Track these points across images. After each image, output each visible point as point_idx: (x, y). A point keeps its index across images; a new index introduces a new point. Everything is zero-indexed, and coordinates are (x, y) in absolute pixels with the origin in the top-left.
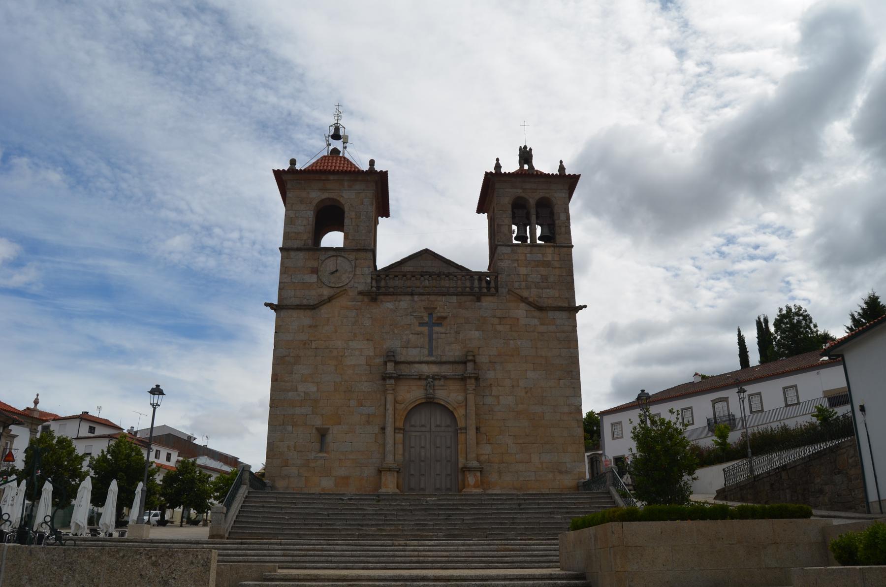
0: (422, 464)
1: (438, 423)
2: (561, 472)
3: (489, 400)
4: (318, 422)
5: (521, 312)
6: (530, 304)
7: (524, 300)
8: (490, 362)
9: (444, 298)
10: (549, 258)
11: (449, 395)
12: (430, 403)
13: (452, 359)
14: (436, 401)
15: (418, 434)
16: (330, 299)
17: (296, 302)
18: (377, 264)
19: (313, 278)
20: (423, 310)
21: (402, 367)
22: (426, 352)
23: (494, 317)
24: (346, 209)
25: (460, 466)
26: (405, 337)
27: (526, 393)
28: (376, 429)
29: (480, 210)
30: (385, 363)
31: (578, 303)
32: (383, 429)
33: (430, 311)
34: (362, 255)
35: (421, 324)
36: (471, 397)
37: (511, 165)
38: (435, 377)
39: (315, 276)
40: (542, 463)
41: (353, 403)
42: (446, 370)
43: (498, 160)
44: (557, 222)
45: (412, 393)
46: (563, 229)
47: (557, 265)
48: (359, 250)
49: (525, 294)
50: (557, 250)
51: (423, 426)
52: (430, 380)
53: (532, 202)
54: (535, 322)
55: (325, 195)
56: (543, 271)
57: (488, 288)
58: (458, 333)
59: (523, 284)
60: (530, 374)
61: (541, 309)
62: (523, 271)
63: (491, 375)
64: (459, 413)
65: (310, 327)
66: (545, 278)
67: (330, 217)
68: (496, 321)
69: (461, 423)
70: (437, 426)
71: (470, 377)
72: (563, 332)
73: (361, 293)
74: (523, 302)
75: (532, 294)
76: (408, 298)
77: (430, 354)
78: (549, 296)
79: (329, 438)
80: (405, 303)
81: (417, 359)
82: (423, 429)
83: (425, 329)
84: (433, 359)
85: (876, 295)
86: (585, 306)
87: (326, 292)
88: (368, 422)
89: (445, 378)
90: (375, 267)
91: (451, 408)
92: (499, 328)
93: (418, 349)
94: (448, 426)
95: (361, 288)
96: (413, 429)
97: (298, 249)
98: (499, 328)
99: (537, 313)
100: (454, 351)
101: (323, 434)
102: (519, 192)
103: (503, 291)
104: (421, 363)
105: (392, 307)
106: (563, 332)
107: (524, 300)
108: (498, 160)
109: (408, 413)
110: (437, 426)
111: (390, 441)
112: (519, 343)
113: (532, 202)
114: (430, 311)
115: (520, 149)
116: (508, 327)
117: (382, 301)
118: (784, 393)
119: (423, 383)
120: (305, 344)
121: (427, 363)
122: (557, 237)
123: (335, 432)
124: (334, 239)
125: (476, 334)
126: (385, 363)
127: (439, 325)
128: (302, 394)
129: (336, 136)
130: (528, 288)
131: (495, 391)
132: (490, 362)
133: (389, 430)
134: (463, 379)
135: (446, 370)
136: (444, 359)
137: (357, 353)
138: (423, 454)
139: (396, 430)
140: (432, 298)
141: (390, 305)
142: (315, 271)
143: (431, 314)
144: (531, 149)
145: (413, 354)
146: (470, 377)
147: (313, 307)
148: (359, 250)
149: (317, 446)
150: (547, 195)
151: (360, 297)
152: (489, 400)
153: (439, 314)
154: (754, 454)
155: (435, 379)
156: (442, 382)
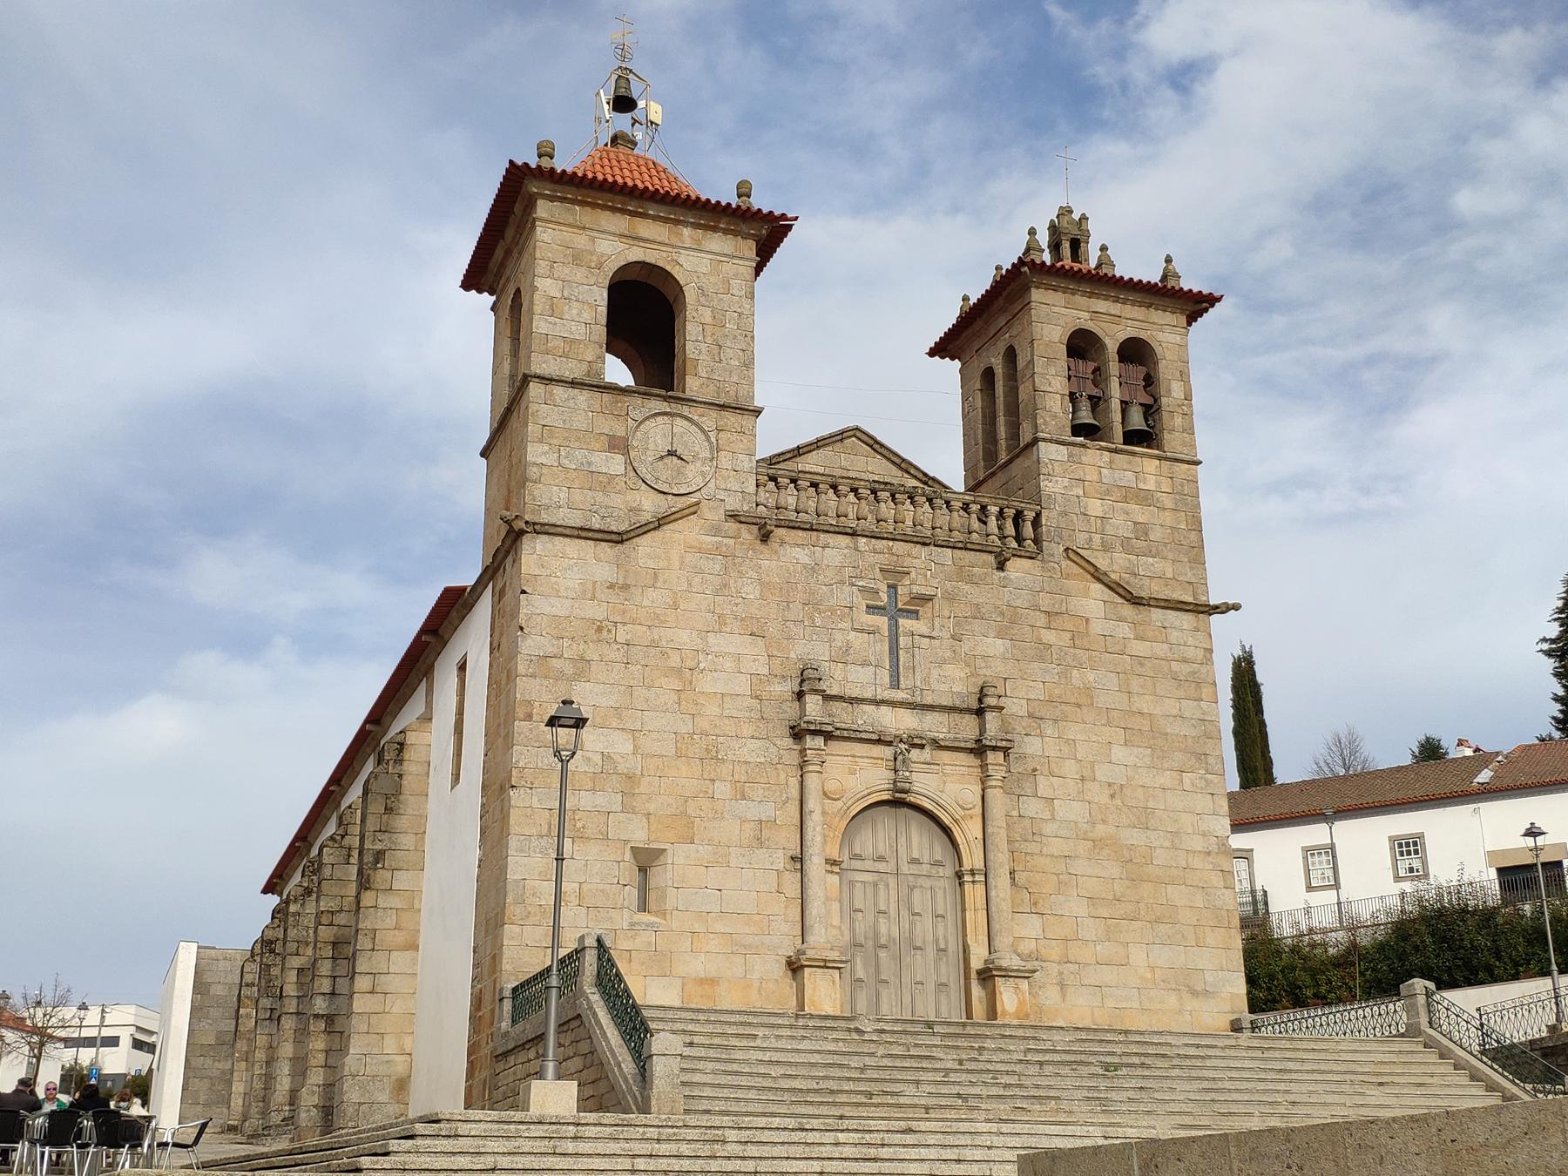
0: (883, 954)
1: (915, 855)
2: (1194, 993)
3: (1031, 807)
4: (639, 834)
5: (1093, 601)
6: (1113, 587)
7: (1098, 576)
8: (1031, 716)
9: (924, 551)
10: (1150, 485)
11: (946, 784)
12: (899, 801)
13: (946, 701)
14: (911, 798)
15: (868, 877)
16: (660, 522)
17: (575, 519)
19: (616, 464)
20: (878, 575)
21: (837, 707)
22: (886, 678)
23: (1036, 608)
24: (690, 295)
25: (976, 964)
26: (838, 636)
27: (1112, 796)
28: (780, 860)
29: (472, 281)
30: (800, 695)
33: (894, 575)
34: (731, 419)
35: (871, 609)
36: (996, 797)
38: (916, 743)
39: (620, 458)
40: (1152, 968)
41: (722, 789)
42: (936, 725)
44: (1164, 400)
45: (857, 774)
46: (1178, 420)
47: (1168, 502)
48: (723, 407)
49: (1102, 562)
51: (881, 859)
53: (1112, 346)
54: (1124, 630)
55: (636, 254)
56: (1141, 514)
57: (1019, 538)
58: (956, 638)
59: (1097, 538)
60: (1119, 753)
61: (1136, 601)
62: (1095, 507)
64: (968, 833)
65: (611, 586)
66: (1142, 530)
68: (1041, 620)
69: (972, 858)
70: (914, 861)
71: (994, 748)
72: (1185, 661)
73: (734, 516)
74: (1099, 580)
75: (1115, 564)
76: (844, 541)
77: (895, 684)
79: (657, 878)
80: (837, 550)
81: (868, 695)
82: (881, 867)
83: (882, 622)
84: (899, 695)
86: (1236, 607)
87: (650, 505)
88: (760, 842)
89: (937, 745)
91: (946, 820)
92: (1049, 636)
93: (872, 669)
94: (938, 864)
95: (733, 503)
96: (857, 864)
97: (573, 384)
98: (1049, 636)
99: (1128, 610)
100: (953, 683)
101: (645, 861)
102: (1083, 320)
103: (1054, 549)
104: (878, 703)
105: (807, 560)
106: (1185, 661)
107: (1098, 576)
110: (914, 861)
111: (816, 890)
112: (1091, 676)
113: (1112, 346)
114: (894, 575)
116: (1068, 635)
117: (783, 543)
118: (1305, 858)
119: (888, 752)
120: (600, 629)
121: (893, 704)
122: (1166, 435)
123: (680, 863)
125: (997, 646)
126: (800, 695)
127: (914, 614)
128: (597, 759)
130: (1106, 548)
131: (1044, 786)
132: (1031, 716)
133: (815, 865)
134: (979, 750)
135: (936, 725)
136: (929, 699)
137: (729, 665)
138: (883, 929)
140: (899, 547)
141: (802, 555)
142: (618, 445)
143: (893, 588)
144: (1084, 218)
145: (860, 680)
146: (994, 748)
147: (618, 538)
148: (723, 407)
149: (633, 893)
150: (1143, 335)
151: (732, 526)
152: (1031, 807)
153: (915, 589)
154: (1561, 972)
155: (914, 746)
156: (927, 754)
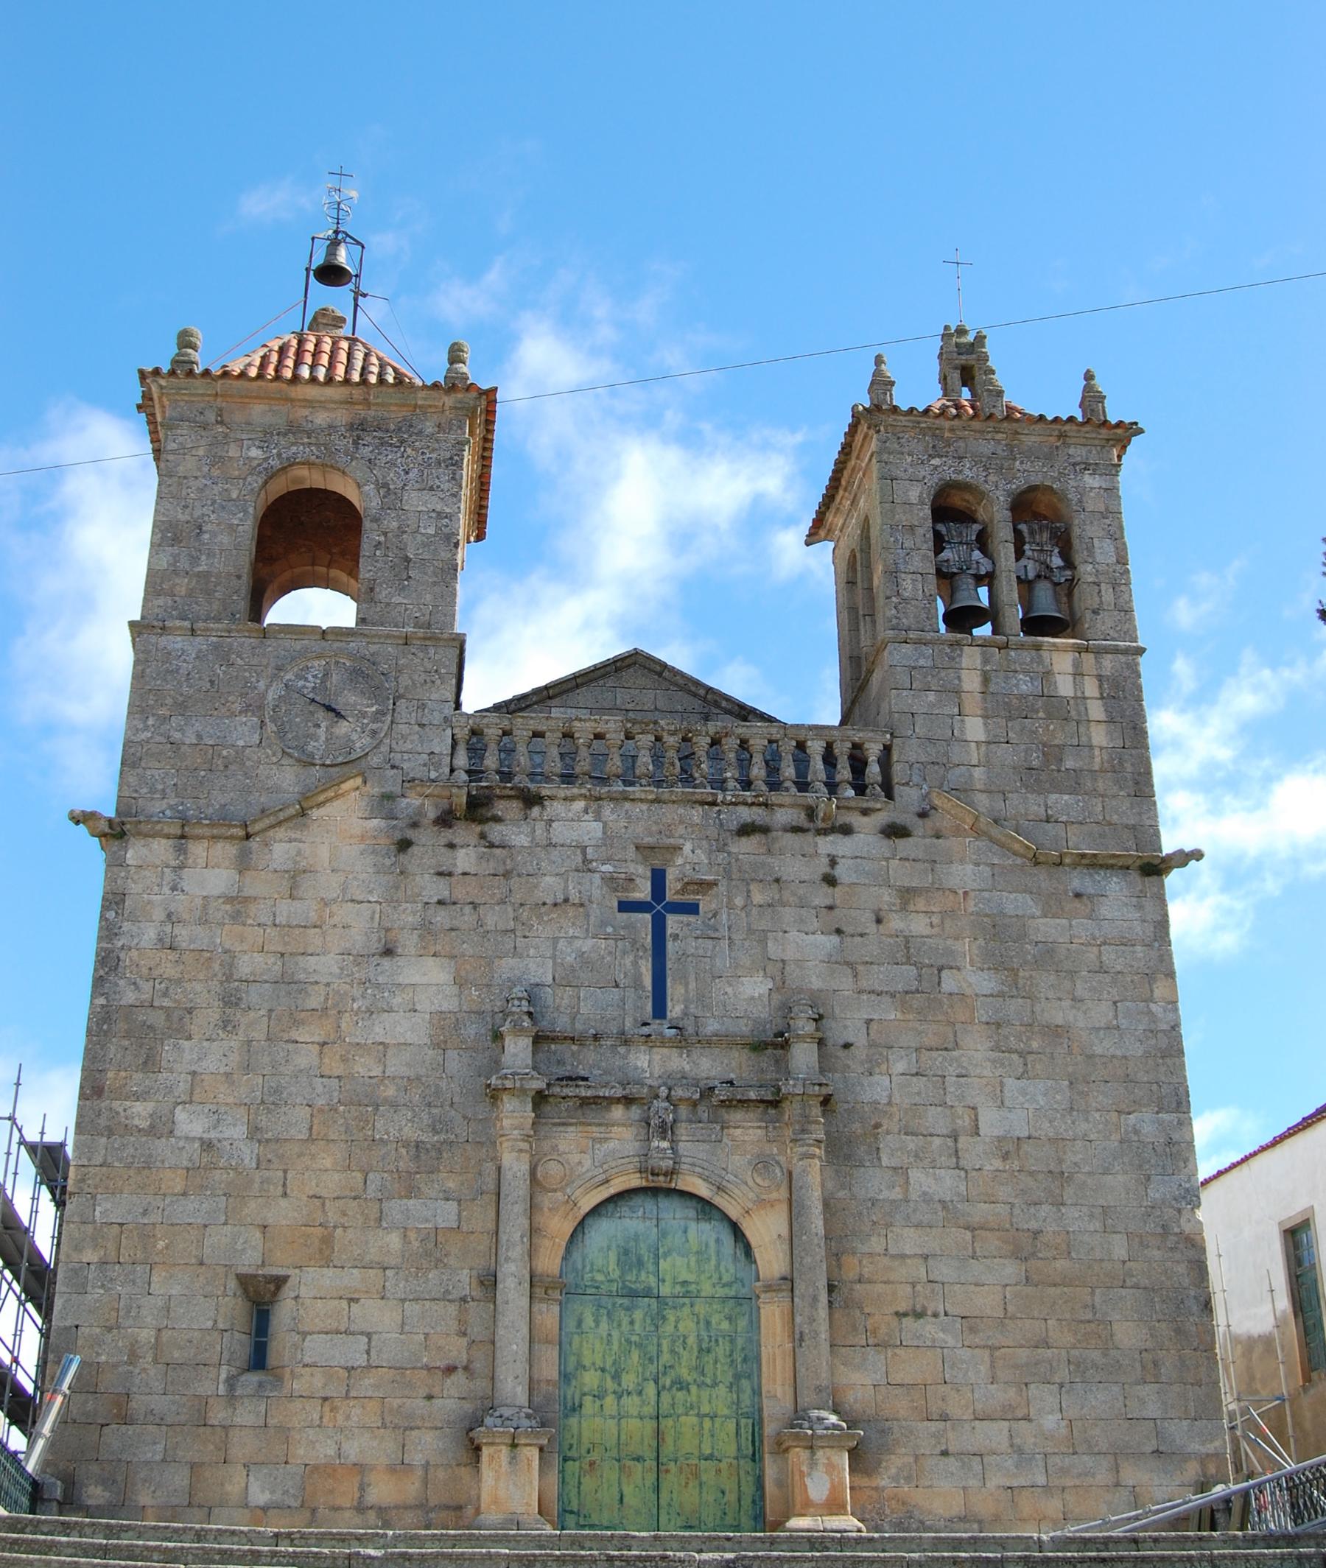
18: (463, 698)
28: (464, 1280)
31: (1169, 845)
32: (489, 1282)
37: (919, 387)
43: (1089, 376)
50: (1089, 659)
52: (660, 1112)
63: (877, 1089)
67: (305, 533)
78: (1072, 818)
79: (283, 1313)
85: (1036, 385)
90: (458, 705)
108: (1089, 376)
109: (581, 1225)
115: (946, 336)
124: (317, 607)
129: (331, 274)
139: (536, 1284)
